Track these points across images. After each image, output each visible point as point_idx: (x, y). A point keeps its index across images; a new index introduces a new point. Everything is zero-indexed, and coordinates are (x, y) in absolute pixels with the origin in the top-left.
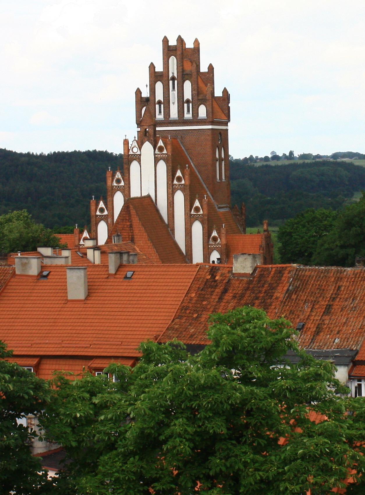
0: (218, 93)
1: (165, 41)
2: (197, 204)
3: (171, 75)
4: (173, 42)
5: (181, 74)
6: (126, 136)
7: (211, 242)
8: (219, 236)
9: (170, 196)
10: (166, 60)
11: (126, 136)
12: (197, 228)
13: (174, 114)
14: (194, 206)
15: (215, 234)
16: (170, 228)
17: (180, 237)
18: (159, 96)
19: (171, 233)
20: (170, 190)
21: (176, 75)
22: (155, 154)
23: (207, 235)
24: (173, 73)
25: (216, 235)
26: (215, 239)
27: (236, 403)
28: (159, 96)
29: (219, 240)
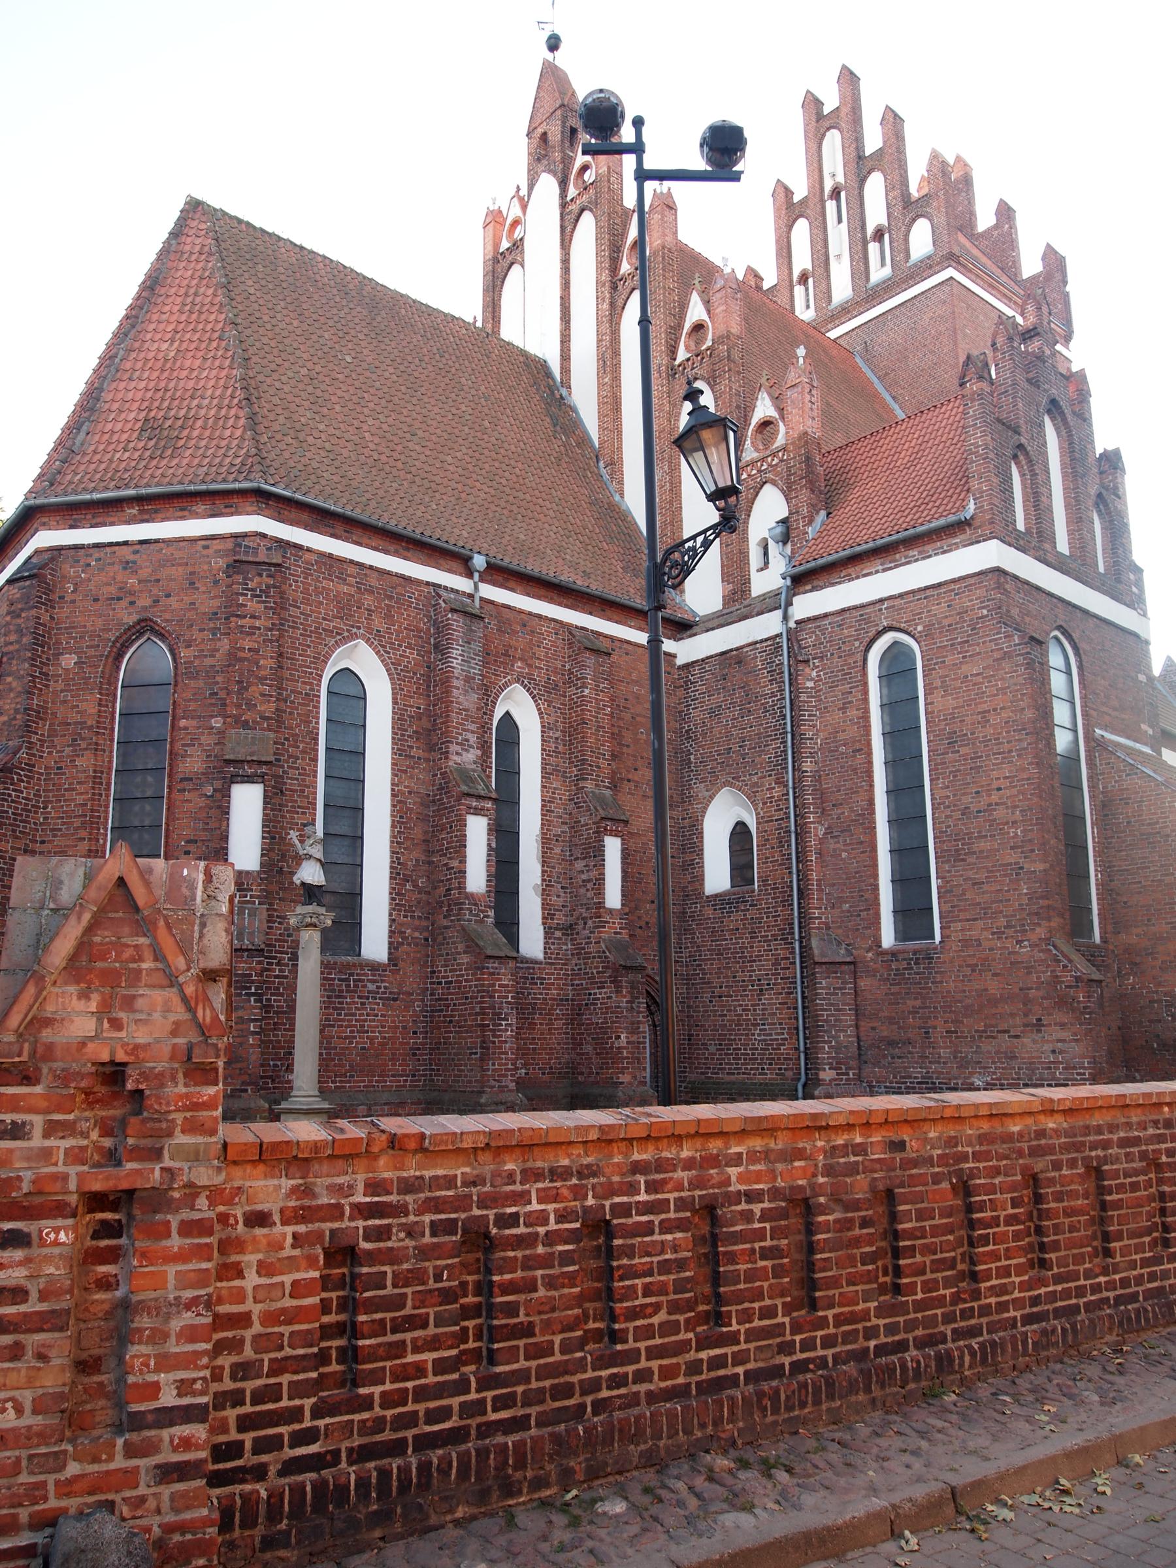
0: (1031, 265)
1: (812, 103)
3: (828, 185)
4: (831, 101)
8: (781, 410)
18: (802, 260)
19: (606, 477)
21: (840, 179)
22: (563, 205)
28: (802, 260)
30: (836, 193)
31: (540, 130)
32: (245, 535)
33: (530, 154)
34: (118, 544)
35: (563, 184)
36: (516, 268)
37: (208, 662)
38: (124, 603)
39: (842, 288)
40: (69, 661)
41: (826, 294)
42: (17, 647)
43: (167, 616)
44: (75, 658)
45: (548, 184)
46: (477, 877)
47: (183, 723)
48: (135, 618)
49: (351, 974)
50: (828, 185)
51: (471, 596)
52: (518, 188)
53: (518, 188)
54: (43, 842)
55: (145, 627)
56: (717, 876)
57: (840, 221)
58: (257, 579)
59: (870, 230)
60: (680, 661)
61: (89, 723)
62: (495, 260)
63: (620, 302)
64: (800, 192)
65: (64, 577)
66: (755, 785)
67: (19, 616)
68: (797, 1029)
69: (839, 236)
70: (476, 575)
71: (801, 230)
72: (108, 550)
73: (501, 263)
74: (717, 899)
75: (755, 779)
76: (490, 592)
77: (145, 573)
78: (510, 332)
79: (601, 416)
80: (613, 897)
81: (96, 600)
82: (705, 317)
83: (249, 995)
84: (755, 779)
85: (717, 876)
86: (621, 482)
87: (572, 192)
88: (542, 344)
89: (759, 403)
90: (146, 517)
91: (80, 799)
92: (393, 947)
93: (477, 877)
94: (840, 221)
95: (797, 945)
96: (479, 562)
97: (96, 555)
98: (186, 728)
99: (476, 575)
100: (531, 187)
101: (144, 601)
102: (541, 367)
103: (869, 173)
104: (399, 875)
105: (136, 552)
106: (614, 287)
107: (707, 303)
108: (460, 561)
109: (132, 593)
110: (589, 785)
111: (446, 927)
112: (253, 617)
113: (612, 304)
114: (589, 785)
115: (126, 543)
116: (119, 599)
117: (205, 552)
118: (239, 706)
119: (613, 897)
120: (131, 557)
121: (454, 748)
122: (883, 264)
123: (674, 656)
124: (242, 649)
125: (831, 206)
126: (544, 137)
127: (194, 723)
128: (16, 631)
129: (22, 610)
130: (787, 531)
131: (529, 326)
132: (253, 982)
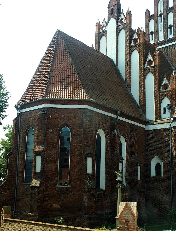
2: (150, 58)
3: (159, 13)
5: (166, 10)
6: (98, 20)
7: (162, 90)
8: (169, 83)
9: (128, 56)
10: (156, 4)
11: (98, 20)
12: (150, 79)
13: (161, 38)
14: (148, 60)
15: (165, 81)
16: (127, 84)
17: (135, 92)
18: (152, 29)
19: (128, 88)
20: (128, 51)
21: (162, 12)
22: (117, 26)
23: (158, 84)
24: (161, 11)
25: (167, 82)
26: (166, 86)
27: (53, 206)
28: (152, 29)
29: (169, 86)
30: (161, 15)
31: (111, 8)
32: (85, 109)
33: (108, 12)
34: (60, 108)
35: (117, 22)
36: (104, 38)
37: (79, 133)
38: (61, 120)
39: (161, 38)
40: (51, 130)
41: (157, 38)
42: (41, 127)
43: (70, 123)
44: (52, 130)
45: (113, 22)
46: (89, 170)
47: (74, 144)
48: (64, 123)
49: (100, 192)
50: (159, 13)
51: (117, 119)
52: (104, 19)
53: (104, 19)
54: (46, 165)
55: (66, 125)
56: (153, 173)
57: (161, 22)
58: (89, 118)
59: (169, 25)
60: (146, 130)
61: (55, 143)
62: (99, 33)
63: (131, 51)
64: (152, 13)
65: (49, 114)
66: (163, 156)
67: (42, 121)
68: (171, 204)
69: (161, 25)
70: (118, 115)
71: (152, 23)
72: (58, 109)
73: (101, 34)
74: (153, 177)
75: (163, 155)
76: (120, 118)
77: (66, 114)
78: (102, 50)
79: (126, 75)
80: (139, 178)
81: (56, 119)
82: (152, 59)
83: (93, 197)
84: (163, 155)
85: (153, 173)
86: (131, 89)
87: (119, 24)
88: (111, 54)
89: (164, 80)
90: (66, 103)
91: (54, 157)
92: (106, 187)
93: (89, 170)
94: (161, 22)
95: (172, 188)
96: (119, 112)
97: (56, 110)
98: (74, 145)
99: (118, 115)
100: (109, 20)
101: (66, 120)
102: (111, 60)
103: (169, 12)
104: (107, 173)
105: (64, 110)
106: (130, 48)
107: (153, 57)
108: (116, 113)
109: (63, 118)
110: (134, 156)
111: (114, 184)
112: (88, 125)
113: (130, 51)
114: (134, 156)
115: (62, 108)
116: (61, 119)
117: (78, 112)
118: (86, 142)
119: (139, 178)
120: (63, 111)
121: (116, 149)
122: (171, 34)
123: (145, 128)
124: (87, 131)
125: (159, 18)
126: (112, 10)
127: (76, 144)
128: (41, 124)
129: (42, 120)
130: (170, 107)
131: (108, 49)
132: (94, 194)
